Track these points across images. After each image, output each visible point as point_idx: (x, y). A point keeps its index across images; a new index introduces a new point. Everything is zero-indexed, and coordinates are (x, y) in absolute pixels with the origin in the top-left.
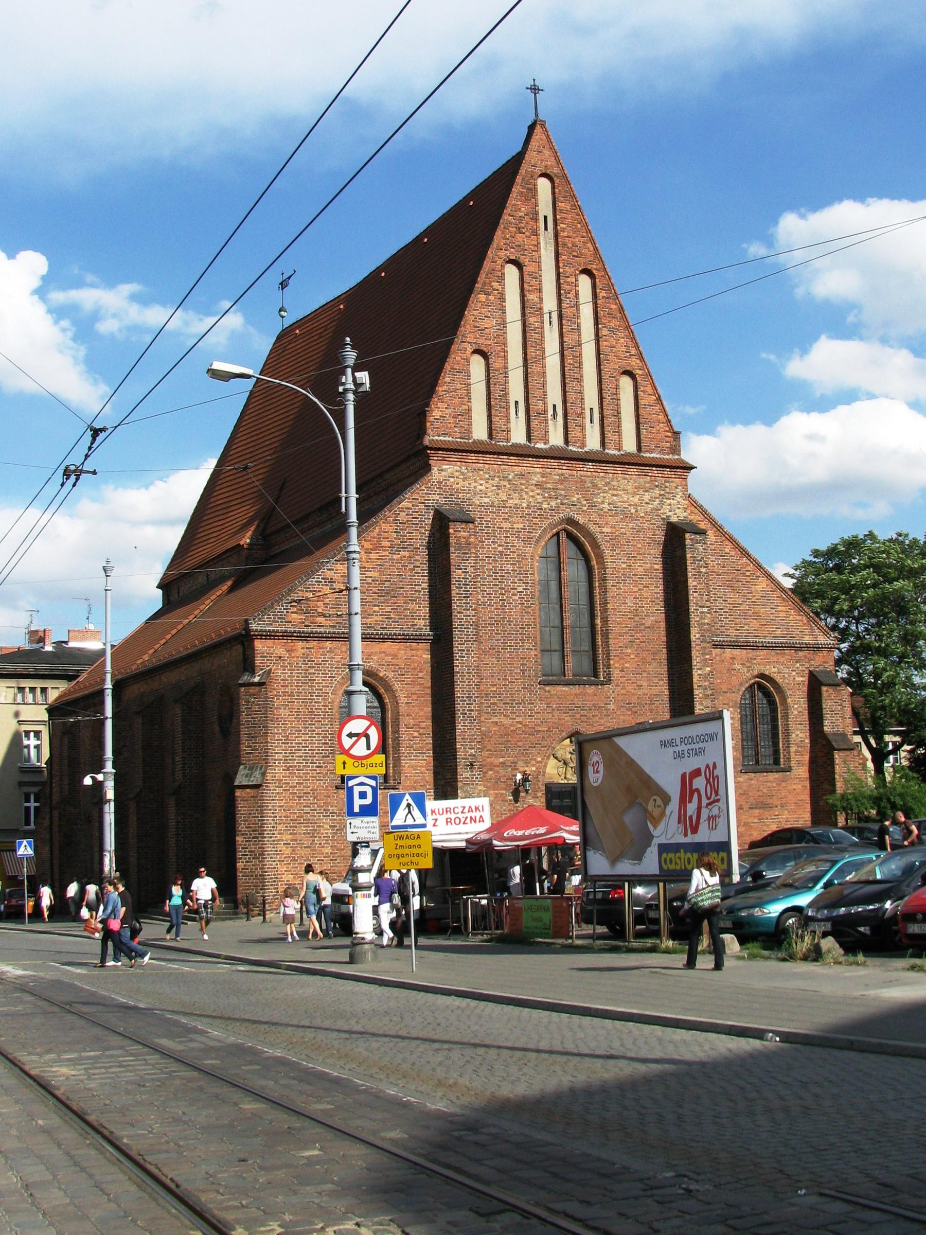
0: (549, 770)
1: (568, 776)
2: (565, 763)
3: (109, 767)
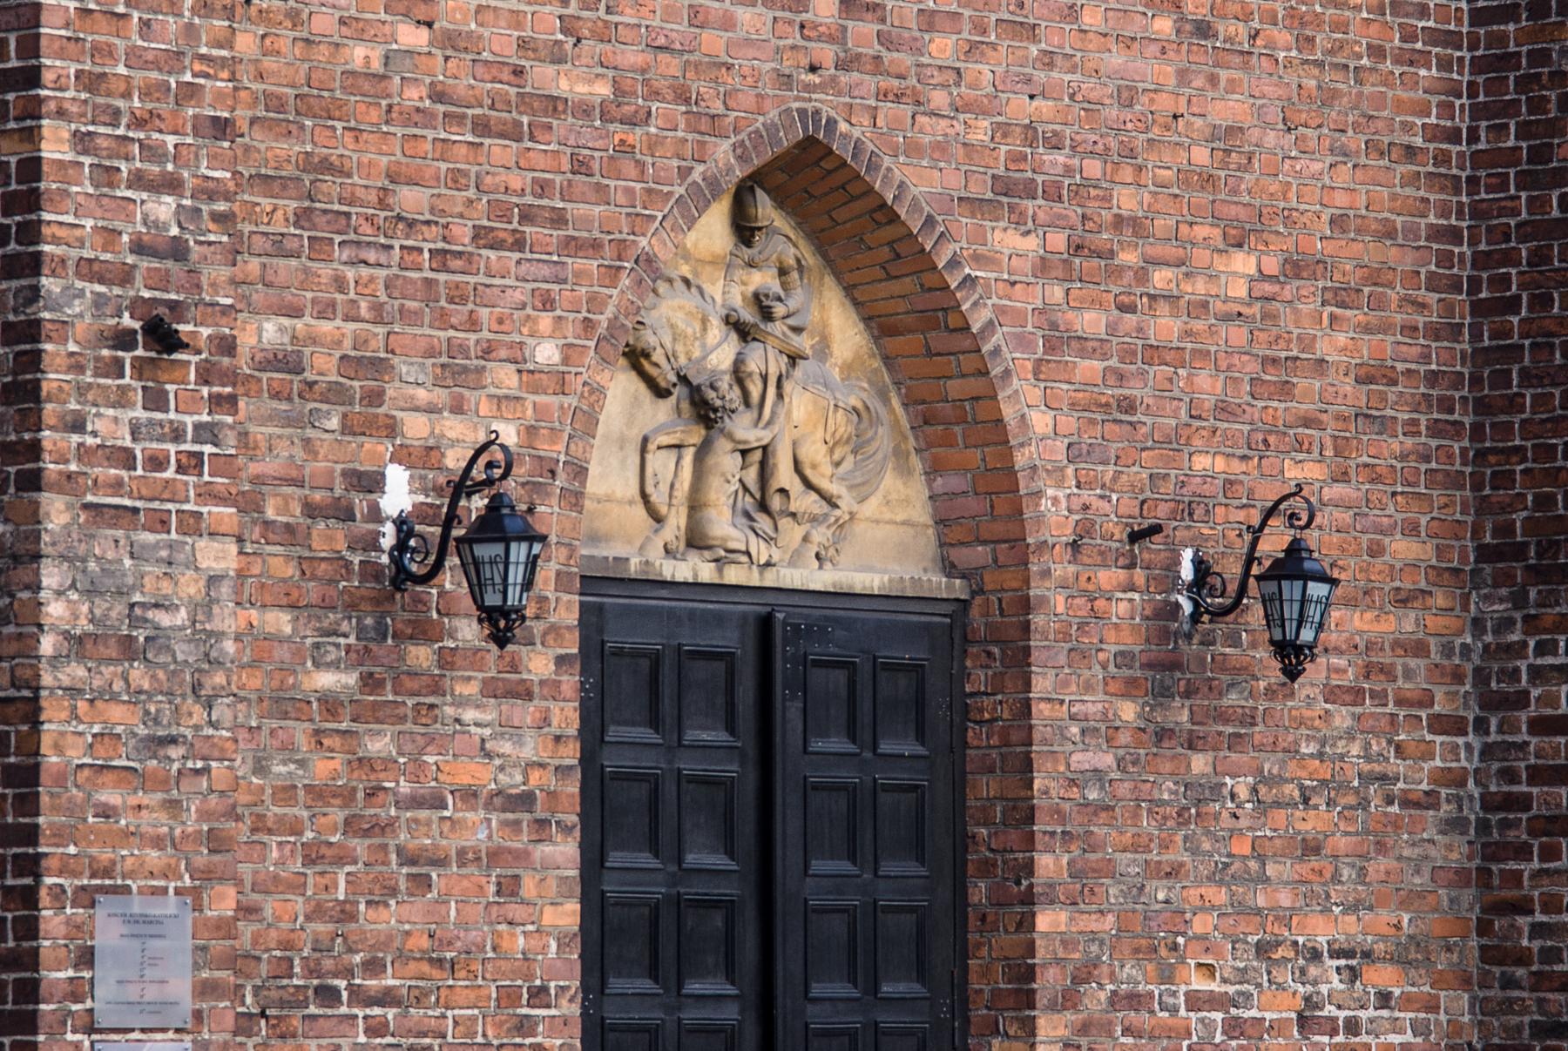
0: (611, 478)
1: (723, 525)
2: (705, 411)
3: (20, 64)
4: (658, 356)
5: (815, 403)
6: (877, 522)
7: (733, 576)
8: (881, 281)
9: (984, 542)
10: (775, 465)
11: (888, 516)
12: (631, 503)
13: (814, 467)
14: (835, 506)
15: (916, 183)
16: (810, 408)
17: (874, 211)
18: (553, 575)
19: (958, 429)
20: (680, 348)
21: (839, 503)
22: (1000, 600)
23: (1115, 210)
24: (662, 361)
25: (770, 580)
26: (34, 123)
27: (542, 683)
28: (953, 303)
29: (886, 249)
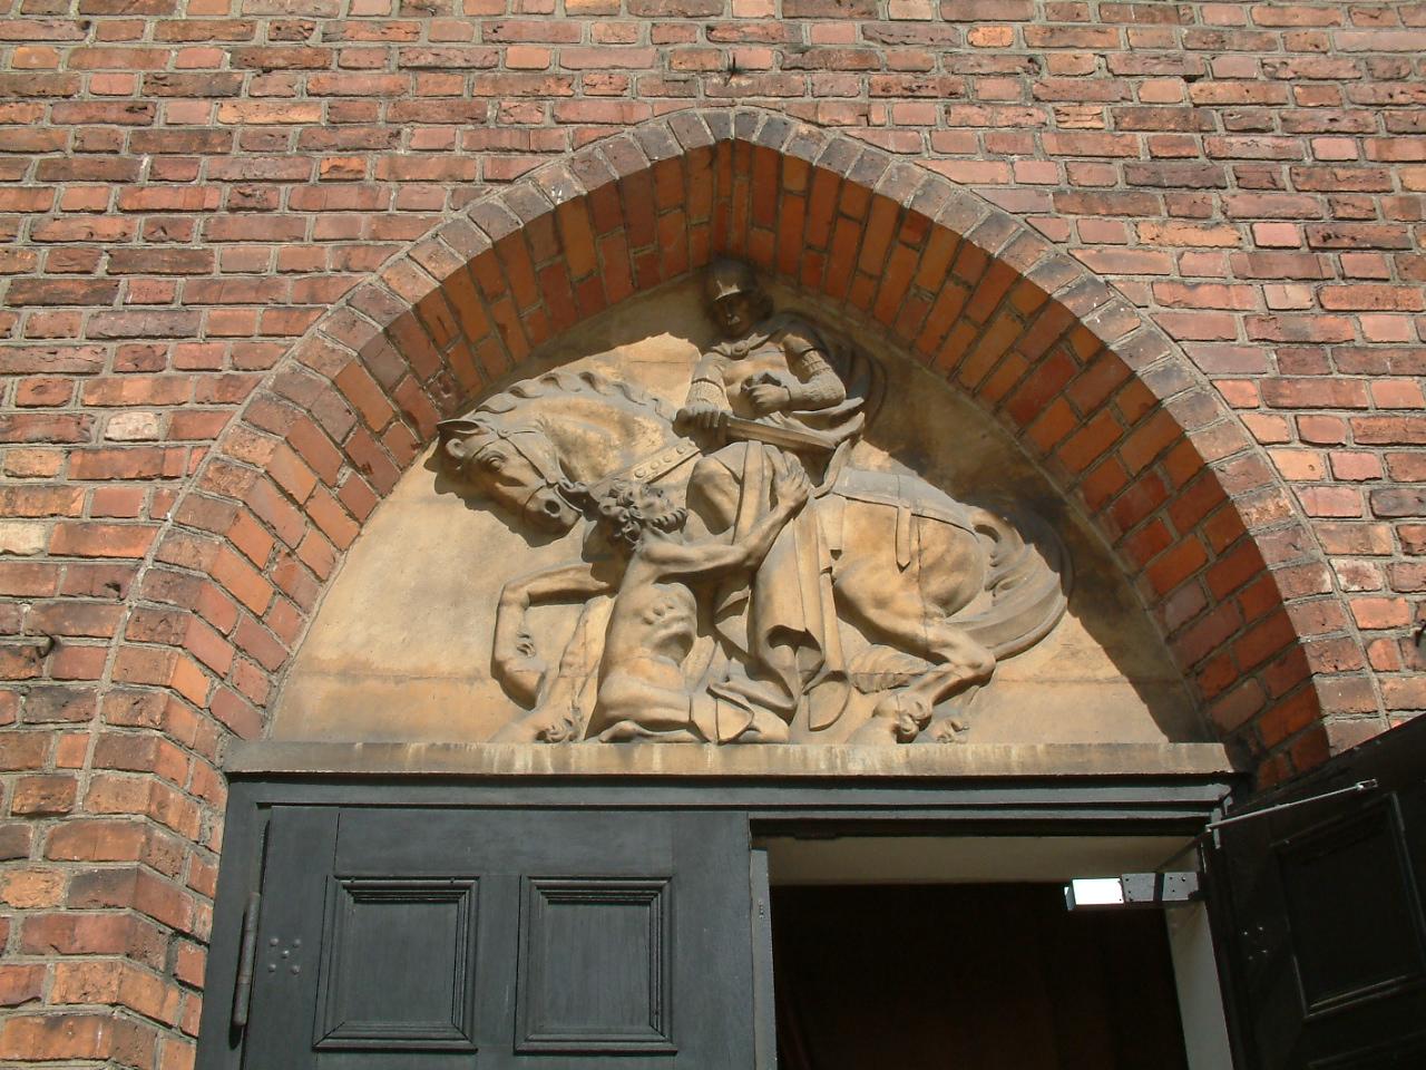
4: (514, 468)
5: (871, 514)
6: (1054, 682)
7: (654, 758)
8: (977, 339)
9: (1249, 672)
10: (769, 597)
11: (1076, 673)
12: (473, 678)
13: (881, 603)
14: (939, 660)
15: (963, 173)
16: (863, 523)
17: (895, 234)
18: (93, 741)
19: (1163, 515)
20: (578, 464)
21: (946, 653)
22: (1288, 753)
23: (1399, 192)
24: (527, 476)
25: (748, 762)
26: (1207, 814)
27: (29, 923)
28: (1068, 322)
29: (950, 285)
